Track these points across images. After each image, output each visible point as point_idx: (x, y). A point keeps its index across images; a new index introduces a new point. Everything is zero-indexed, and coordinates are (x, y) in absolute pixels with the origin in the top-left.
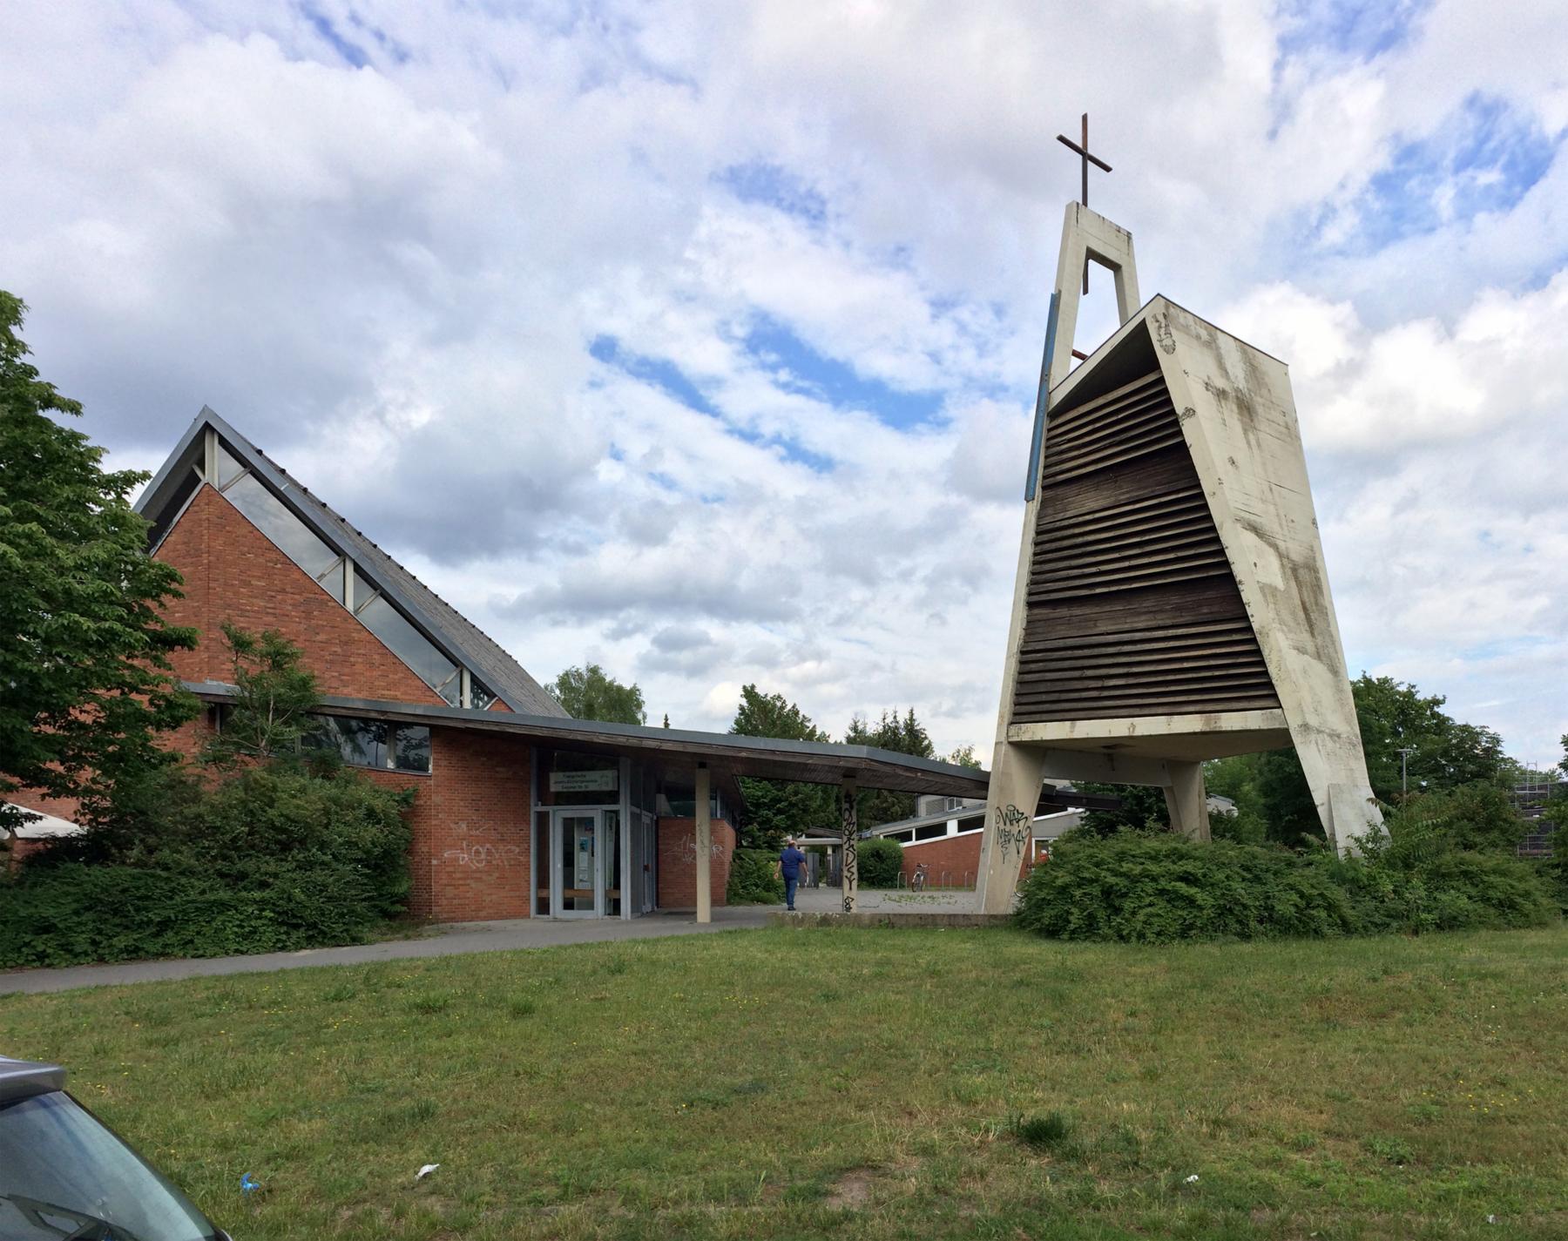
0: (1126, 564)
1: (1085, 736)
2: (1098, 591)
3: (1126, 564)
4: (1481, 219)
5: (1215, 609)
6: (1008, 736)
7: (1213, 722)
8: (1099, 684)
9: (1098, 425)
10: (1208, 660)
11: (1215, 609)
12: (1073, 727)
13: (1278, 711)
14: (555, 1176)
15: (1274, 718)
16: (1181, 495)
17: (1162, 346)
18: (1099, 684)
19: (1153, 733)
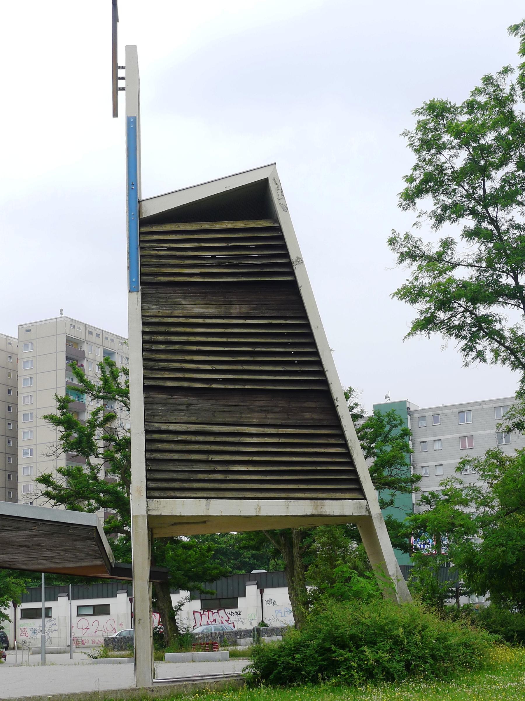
0: (239, 367)
1: (219, 514)
2: (214, 386)
3: (239, 367)
4: (417, 201)
5: (315, 416)
6: (148, 510)
7: (319, 507)
8: (224, 468)
9: (203, 245)
10: (280, 466)
11: (315, 416)
12: (208, 505)
13: (363, 502)
14: (453, 658)
15: (361, 506)
16: (288, 322)
17: (280, 204)
18: (224, 468)
19: (275, 514)
